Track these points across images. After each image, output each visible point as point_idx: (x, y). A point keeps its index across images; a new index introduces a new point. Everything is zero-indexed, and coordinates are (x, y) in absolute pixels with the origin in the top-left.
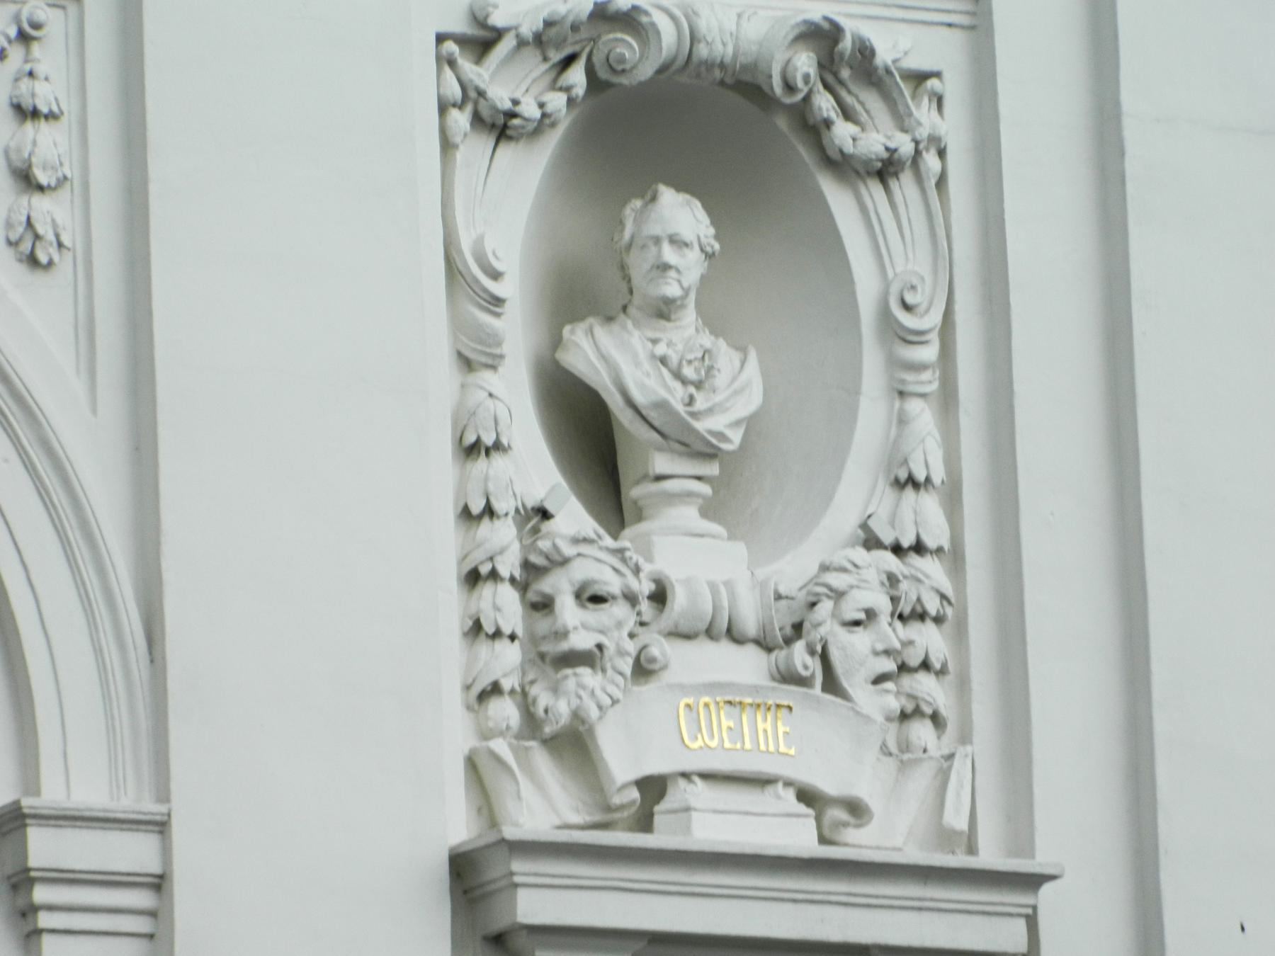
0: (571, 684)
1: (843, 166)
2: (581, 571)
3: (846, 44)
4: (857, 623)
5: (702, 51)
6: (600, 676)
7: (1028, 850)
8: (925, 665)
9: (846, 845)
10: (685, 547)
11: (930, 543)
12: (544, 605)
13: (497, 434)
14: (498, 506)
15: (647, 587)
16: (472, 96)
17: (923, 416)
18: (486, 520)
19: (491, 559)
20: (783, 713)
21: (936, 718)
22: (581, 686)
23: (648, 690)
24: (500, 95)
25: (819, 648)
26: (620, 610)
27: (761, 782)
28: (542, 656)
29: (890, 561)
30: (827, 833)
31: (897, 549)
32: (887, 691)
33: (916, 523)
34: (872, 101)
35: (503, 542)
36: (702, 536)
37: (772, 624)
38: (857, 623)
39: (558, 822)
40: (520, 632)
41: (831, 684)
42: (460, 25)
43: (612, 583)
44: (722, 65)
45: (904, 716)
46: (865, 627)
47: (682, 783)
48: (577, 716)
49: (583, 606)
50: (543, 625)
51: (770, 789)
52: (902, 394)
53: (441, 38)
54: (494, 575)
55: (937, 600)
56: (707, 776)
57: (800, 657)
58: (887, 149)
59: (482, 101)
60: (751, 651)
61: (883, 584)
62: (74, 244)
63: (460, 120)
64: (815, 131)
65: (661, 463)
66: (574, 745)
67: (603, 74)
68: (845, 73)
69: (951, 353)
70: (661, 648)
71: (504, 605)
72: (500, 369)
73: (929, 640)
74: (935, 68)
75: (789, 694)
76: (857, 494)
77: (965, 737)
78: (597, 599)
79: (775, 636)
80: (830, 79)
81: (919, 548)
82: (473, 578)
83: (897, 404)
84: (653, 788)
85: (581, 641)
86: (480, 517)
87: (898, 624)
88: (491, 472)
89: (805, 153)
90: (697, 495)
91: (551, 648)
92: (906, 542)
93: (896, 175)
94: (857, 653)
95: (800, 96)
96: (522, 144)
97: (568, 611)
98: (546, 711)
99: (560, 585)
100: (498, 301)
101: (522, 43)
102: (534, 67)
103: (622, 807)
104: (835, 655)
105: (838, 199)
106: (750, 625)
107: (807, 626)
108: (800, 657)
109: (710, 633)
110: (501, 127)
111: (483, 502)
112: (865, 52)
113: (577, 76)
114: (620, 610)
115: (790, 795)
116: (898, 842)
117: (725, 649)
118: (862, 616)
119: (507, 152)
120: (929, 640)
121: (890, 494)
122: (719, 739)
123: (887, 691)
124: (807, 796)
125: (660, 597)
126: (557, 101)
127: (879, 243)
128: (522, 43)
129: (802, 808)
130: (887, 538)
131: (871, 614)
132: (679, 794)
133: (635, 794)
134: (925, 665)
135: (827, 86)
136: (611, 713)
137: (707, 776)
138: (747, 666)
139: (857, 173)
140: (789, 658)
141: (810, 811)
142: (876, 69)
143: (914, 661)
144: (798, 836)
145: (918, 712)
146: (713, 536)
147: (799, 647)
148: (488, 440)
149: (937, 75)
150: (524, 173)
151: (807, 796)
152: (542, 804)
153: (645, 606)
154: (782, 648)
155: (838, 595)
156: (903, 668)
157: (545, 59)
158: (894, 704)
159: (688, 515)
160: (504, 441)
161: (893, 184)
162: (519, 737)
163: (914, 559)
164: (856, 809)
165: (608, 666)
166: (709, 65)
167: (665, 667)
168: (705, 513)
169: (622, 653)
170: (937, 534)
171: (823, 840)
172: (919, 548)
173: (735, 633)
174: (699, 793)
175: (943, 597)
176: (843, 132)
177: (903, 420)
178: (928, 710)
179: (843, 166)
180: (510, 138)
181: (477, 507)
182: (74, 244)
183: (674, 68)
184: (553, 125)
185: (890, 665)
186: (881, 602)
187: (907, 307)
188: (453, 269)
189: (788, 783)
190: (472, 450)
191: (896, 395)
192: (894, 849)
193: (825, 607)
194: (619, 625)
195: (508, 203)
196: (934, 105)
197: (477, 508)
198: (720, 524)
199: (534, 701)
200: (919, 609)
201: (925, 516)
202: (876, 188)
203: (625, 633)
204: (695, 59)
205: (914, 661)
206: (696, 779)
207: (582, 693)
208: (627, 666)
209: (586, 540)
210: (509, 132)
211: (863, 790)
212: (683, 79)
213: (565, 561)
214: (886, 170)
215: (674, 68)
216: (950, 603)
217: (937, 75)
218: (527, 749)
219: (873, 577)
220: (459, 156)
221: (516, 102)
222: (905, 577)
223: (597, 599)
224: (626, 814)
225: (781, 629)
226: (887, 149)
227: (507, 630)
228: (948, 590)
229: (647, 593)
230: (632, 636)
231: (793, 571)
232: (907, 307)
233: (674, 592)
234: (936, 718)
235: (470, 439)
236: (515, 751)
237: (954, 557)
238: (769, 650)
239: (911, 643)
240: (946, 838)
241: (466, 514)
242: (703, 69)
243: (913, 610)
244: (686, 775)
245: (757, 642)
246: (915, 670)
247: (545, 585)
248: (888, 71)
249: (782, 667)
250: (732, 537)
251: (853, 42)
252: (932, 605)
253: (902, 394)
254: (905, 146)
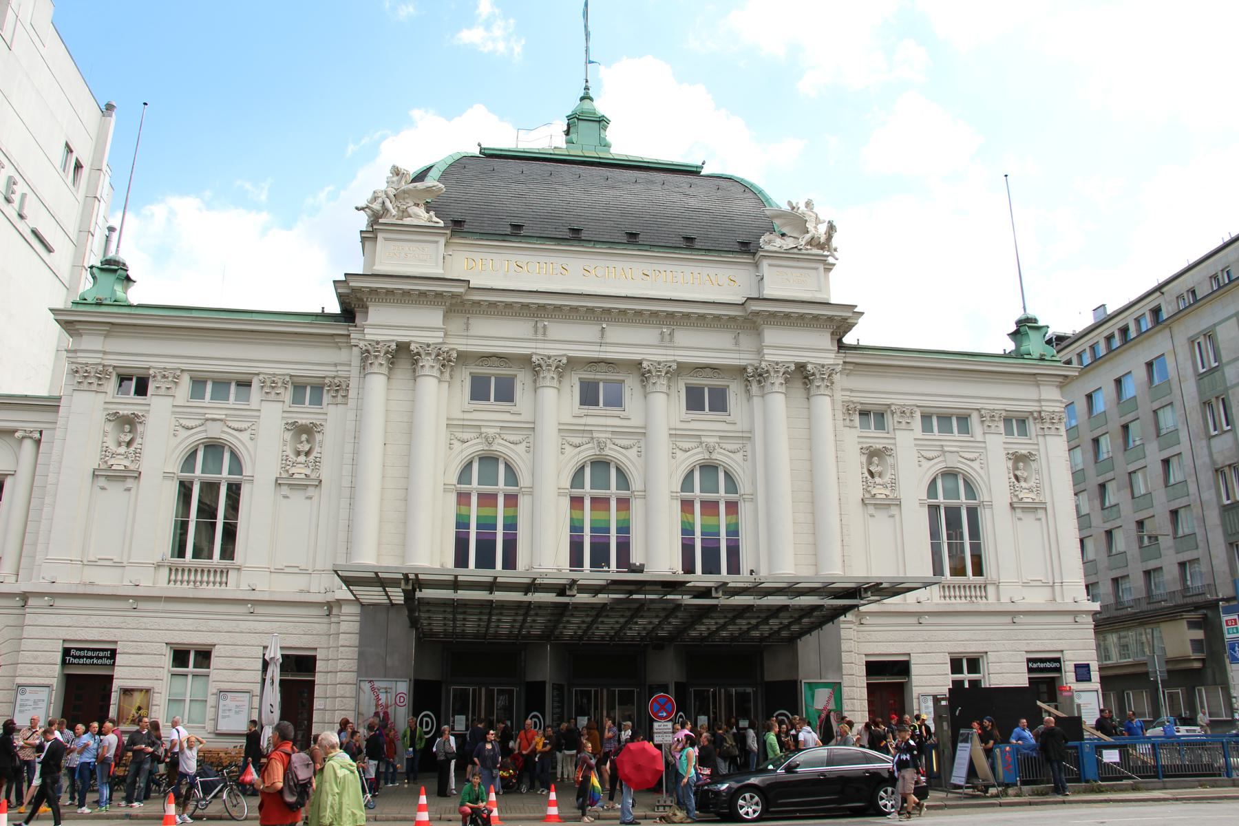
150: (290, 433)
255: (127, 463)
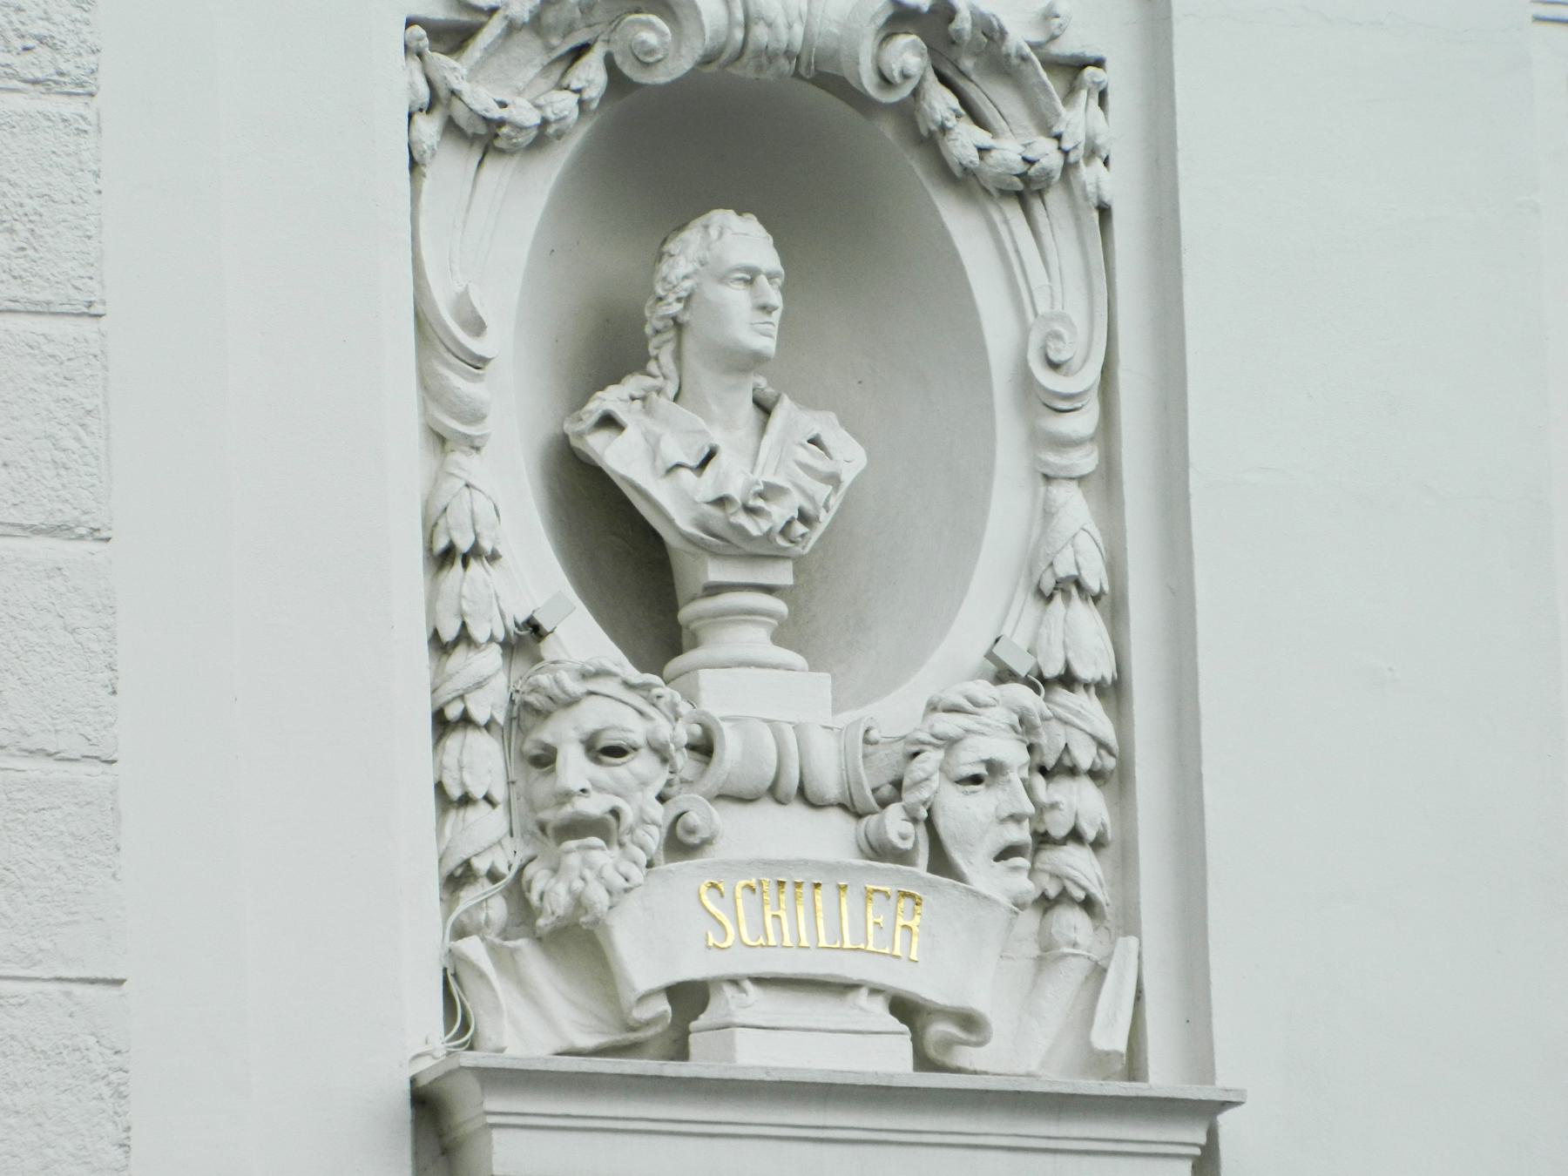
0: (574, 860)
1: (964, 181)
2: (593, 716)
3: (963, 22)
4: (976, 780)
5: (761, 34)
6: (616, 850)
7: (1206, 1072)
8: (1075, 836)
9: (959, 1070)
10: (749, 683)
11: (1084, 672)
12: (545, 760)
13: (477, 535)
14: (479, 632)
15: (684, 733)
16: (437, 99)
17: (1074, 506)
18: (461, 651)
19: (461, 697)
20: (905, 904)
21: (1088, 904)
22: (586, 863)
23: (684, 867)
24: (481, 97)
25: (924, 814)
26: (643, 764)
27: (844, 988)
28: (542, 827)
29: (1021, 694)
30: (932, 1052)
31: (1039, 682)
32: (1016, 869)
33: (1065, 647)
34: (995, 96)
35: (486, 679)
36: (776, 667)
37: (860, 784)
38: (976, 780)
39: (561, 1045)
40: (499, 794)
41: (941, 862)
42: (439, 11)
43: (634, 729)
44: (788, 54)
45: (1046, 903)
46: (988, 786)
47: (729, 991)
48: (579, 903)
49: (596, 761)
50: (543, 787)
51: (851, 996)
52: (1047, 478)
53: (410, 23)
54: (466, 720)
55: (1094, 750)
56: (759, 981)
57: (895, 825)
58: (1025, 160)
59: (456, 102)
60: (836, 818)
61: (1013, 728)
62: (1115, 566)
63: (429, 128)
64: (930, 143)
65: (716, 572)
66: (579, 942)
67: (628, 69)
68: (968, 64)
69: (1118, 428)
70: (702, 815)
71: (482, 761)
72: (484, 451)
73: (1081, 802)
74: (1091, 53)
75: (888, 876)
76: (987, 611)
77: (1130, 924)
78: (617, 752)
79: (865, 798)
80: (949, 71)
81: (1068, 680)
82: (442, 725)
83: (1042, 489)
84: (689, 998)
85: (594, 806)
86: (456, 643)
87: (1039, 780)
88: (465, 590)
89: (915, 165)
90: (768, 614)
91: (552, 816)
92: (1053, 669)
93: (1040, 194)
94: (974, 819)
95: (906, 91)
96: (517, 158)
97: (574, 768)
98: (541, 898)
99: (564, 733)
100: (478, 363)
101: (512, 28)
102: (529, 58)
103: (648, 1024)
104: (944, 825)
105: (962, 226)
106: (829, 783)
107: (906, 782)
108: (895, 825)
109: (773, 792)
110: (486, 138)
111: (458, 624)
112: (992, 33)
113: (591, 75)
114: (643, 764)
115: (879, 1007)
116: (1034, 1068)
117: (797, 812)
118: (981, 770)
119: (497, 172)
120: (1081, 802)
121: (1032, 608)
122: (803, 934)
123: (1016, 869)
124: (905, 1009)
125: (704, 748)
126: (564, 104)
127: (1013, 283)
128: (512, 28)
129: (894, 1023)
130: (1023, 667)
131: (994, 768)
132: (725, 1005)
133: (663, 1006)
134: (1075, 836)
135: (944, 80)
136: (632, 901)
137: (759, 981)
138: (832, 837)
139: (986, 191)
140: (881, 825)
141: (905, 1028)
142: (1008, 55)
143: (1059, 831)
144: (889, 1057)
145: (1064, 897)
146: (789, 668)
147: (894, 812)
148: (464, 545)
149: (1099, 63)
151: (905, 1009)
152: (536, 1017)
153: (683, 760)
154: (872, 813)
155: (950, 743)
156: (1043, 839)
157: (550, 48)
158: (1025, 886)
159: (753, 640)
160: (487, 545)
161: (1037, 206)
162: (505, 934)
163: (1062, 695)
164: (970, 1022)
165: (626, 839)
166: (768, 56)
167: (706, 842)
168: (778, 639)
169: (643, 821)
170: (1095, 664)
171: (923, 1062)
172: (1068, 680)
173: (808, 791)
174: (756, 1004)
175: (1101, 745)
176: (964, 141)
177: (1048, 514)
178: (1080, 895)
179: (964, 181)
180: (501, 152)
181: (449, 632)
182: (1115, 566)
183: (725, 56)
184: (559, 135)
185: (1021, 834)
186: (1013, 753)
187: (1054, 366)
188: (423, 323)
189: (875, 991)
190: (444, 558)
191: (1041, 481)
192: (1028, 1075)
193: (931, 759)
194: (644, 784)
195: (501, 240)
196: (1094, 102)
197: (449, 633)
198: (799, 651)
199: (530, 882)
200: (1067, 762)
201: (1081, 639)
202: (1014, 212)
203: (652, 793)
204: (751, 46)
205: (1059, 831)
206: (748, 985)
207: (588, 874)
208: (654, 839)
209: (600, 673)
210: (499, 143)
211: (978, 1001)
212: (746, 70)
213: (572, 702)
214: (1025, 190)
215: (725, 56)
216: (1110, 752)
217: (1099, 63)
218: (513, 951)
219: (1000, 716)
220: (430, 171)
221: (503, 105)
222: (1044, 719)
223: (617, 752)
224: (659, 1029)
225: (874, 791)
226: (1025, 160)
227: (478, 792)
228: (1107, 731)
229: (685, 739)
230: (662, 798)
231: (897, 714)
232: (1054, 366)
233: (722, 736)
234: (1088, 904)
235: (441, 544)
236: (493, 950)
237: (1113, 692)
238: (859, 816)
239: (1054, 806)
240: (1098, 1062)
241: (436, 641)
242: (764, 60)
243: (1060, 760)
244: (735, 982)
245: (842, 806)
246: (1063, 842)
247: (547, 733)
248: (1024, 59)
249: (872, 838)
250: (813, 667)
251: (974, 25)
252: (1085, 756)
253: (1047, 478)
254: (1048, 155)
255: (941, 945)
